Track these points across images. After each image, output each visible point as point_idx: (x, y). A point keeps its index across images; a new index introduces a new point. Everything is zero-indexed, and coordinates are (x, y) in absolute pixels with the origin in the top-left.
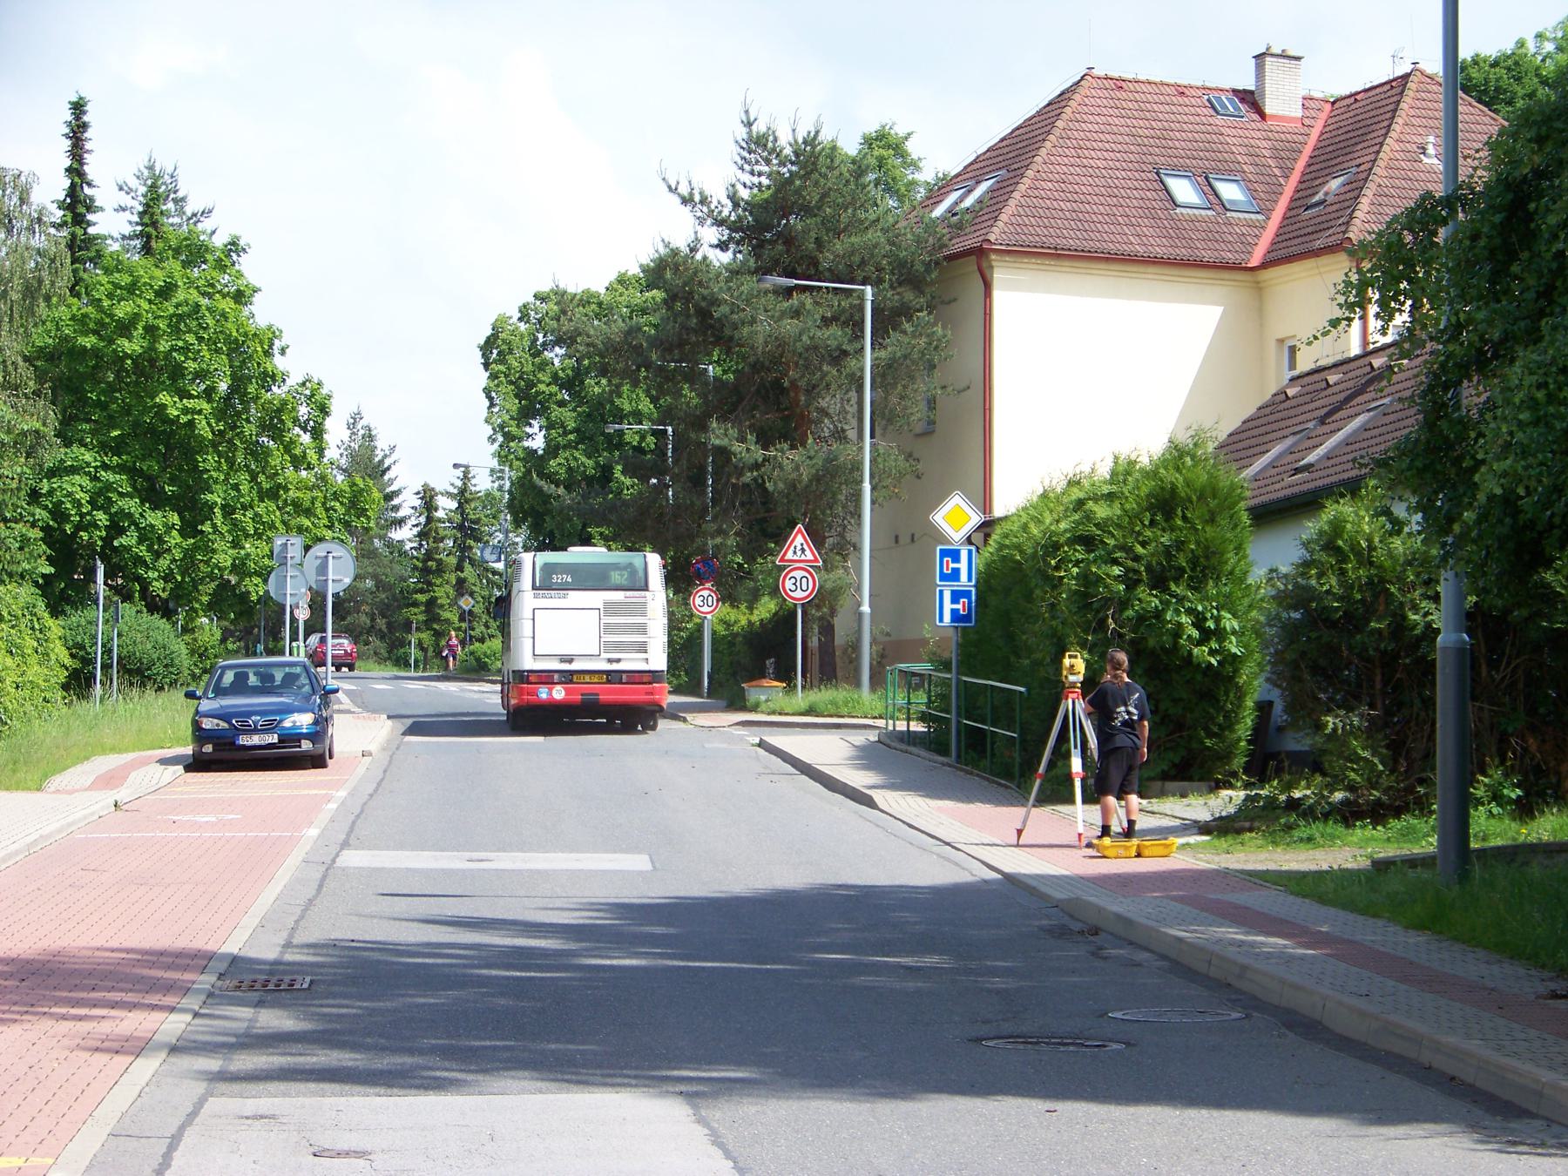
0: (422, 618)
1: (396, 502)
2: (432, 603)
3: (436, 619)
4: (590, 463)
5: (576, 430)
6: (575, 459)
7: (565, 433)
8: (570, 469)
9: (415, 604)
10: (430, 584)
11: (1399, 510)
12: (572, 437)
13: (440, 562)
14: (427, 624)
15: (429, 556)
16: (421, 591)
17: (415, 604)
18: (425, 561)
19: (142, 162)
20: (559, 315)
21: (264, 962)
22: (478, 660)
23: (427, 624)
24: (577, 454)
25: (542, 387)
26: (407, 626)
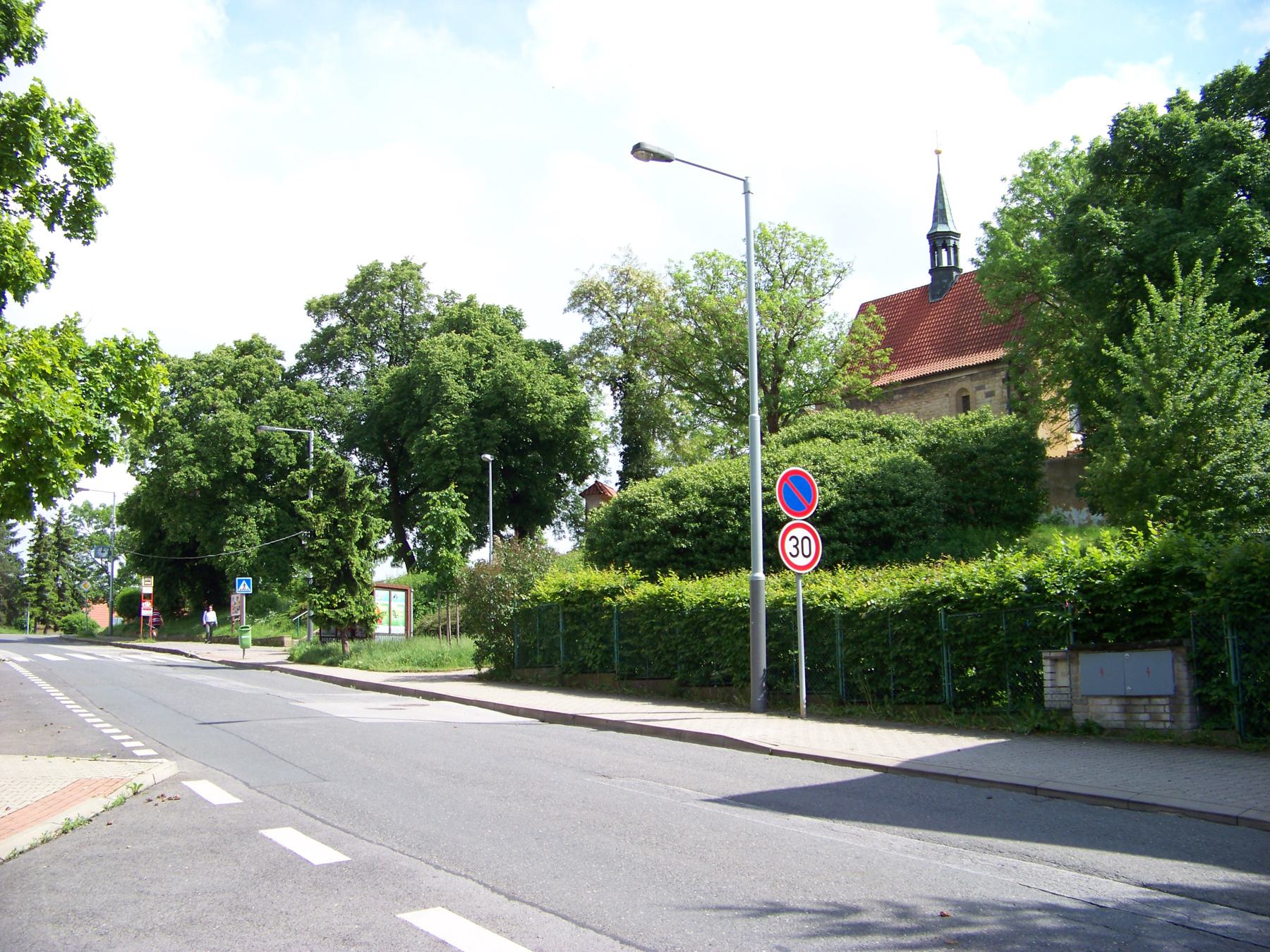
0: (35, 598)
1: (13, 530)
2: (41, 589)
3: (44, 598)
4: (205, 476)
5: (195, 451)
6: (193, 473)
7: (186, 453)
8: (189, 480)
9: (30, 590)
10: (40, 577)
11: (55, 598)
12: (191, 456)
13: (47, 563)
14: (38, 603)
15: (40, 560)
16: (34, 581)
17: (30, 590)
18: (37, 563)
19: (26, 304)
20: (405, 279)
21: (214, 781)
22: (70, 625)
23: (38, 603)
24: (194, 469)
25: (166, 419)
26: (24, 603)
